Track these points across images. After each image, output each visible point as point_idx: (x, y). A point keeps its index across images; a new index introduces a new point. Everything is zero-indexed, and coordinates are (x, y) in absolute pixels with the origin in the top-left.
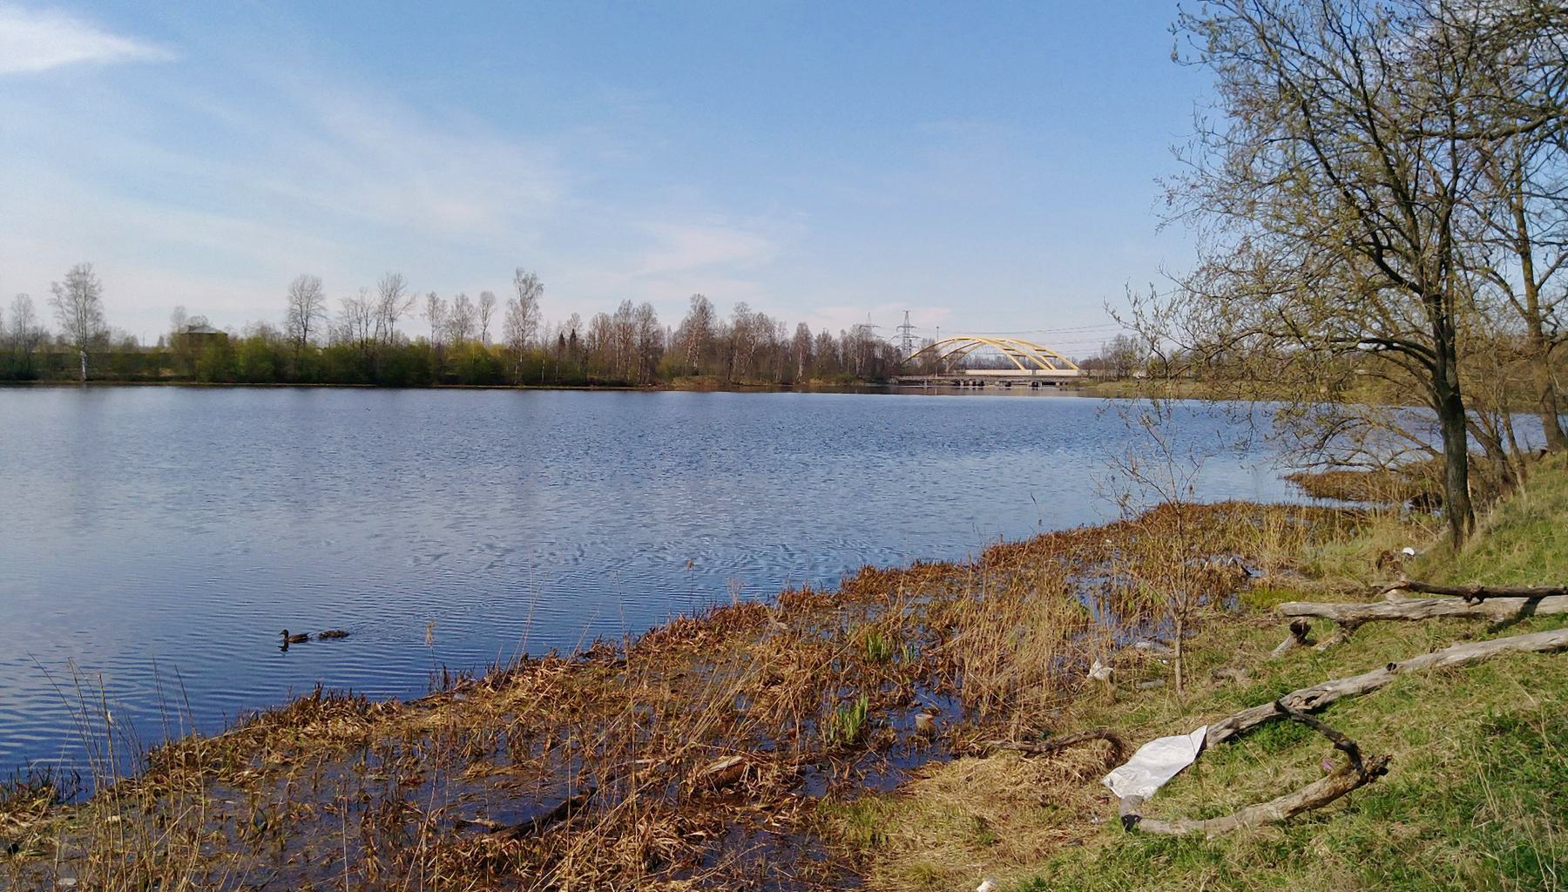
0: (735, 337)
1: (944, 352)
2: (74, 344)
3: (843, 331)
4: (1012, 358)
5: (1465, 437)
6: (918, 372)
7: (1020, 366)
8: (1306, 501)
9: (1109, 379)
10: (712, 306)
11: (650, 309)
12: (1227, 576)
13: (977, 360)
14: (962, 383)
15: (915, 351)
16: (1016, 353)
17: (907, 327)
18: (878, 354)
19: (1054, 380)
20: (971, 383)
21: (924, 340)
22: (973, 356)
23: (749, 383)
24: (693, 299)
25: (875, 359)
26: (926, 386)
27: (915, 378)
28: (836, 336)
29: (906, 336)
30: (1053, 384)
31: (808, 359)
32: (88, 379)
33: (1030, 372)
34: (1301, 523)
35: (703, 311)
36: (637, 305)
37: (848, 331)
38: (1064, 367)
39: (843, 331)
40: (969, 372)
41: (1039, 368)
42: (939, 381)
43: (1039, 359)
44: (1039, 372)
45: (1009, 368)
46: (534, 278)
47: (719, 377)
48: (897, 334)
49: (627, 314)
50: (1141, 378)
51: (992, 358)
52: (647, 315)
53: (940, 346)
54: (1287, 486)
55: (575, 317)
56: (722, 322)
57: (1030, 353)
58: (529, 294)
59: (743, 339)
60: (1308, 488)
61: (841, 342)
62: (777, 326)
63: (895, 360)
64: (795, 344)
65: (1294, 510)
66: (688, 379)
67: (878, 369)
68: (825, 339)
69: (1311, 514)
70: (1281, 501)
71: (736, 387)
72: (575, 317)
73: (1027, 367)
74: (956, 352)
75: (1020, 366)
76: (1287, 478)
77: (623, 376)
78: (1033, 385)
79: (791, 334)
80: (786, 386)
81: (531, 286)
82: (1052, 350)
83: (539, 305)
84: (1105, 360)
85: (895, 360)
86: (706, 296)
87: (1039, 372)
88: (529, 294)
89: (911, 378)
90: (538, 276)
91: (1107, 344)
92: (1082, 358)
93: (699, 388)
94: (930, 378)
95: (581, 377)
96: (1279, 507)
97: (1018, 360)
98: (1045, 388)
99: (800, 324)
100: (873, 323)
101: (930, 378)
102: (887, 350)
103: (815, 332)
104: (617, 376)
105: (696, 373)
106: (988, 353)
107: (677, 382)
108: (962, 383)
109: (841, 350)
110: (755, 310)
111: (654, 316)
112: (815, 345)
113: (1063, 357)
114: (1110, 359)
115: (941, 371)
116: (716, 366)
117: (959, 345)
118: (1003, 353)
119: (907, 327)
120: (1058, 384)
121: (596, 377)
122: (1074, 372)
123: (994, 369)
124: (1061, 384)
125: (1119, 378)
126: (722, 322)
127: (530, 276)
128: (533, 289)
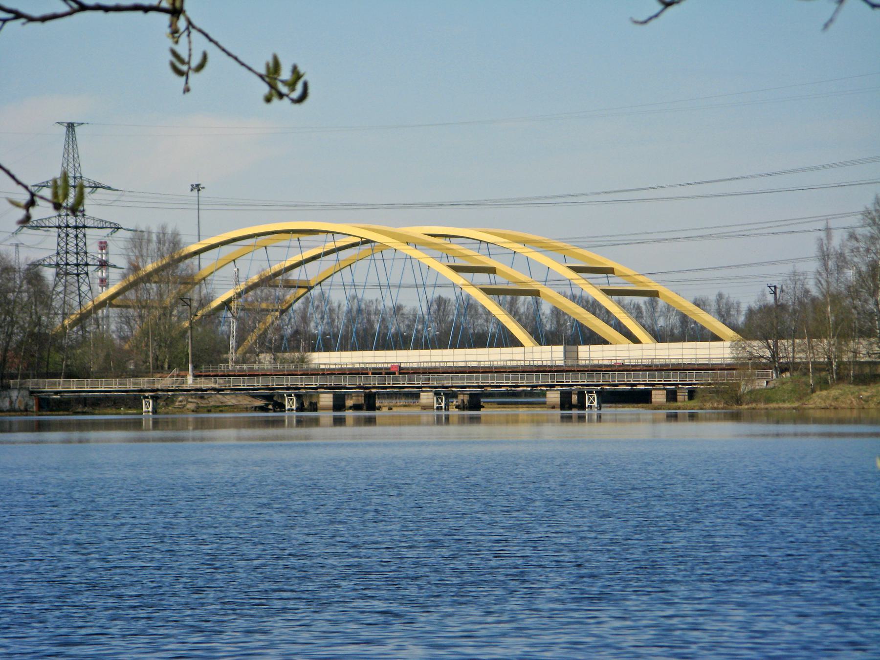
2: (865, 372)
5: (741, 336)
13: (358, 313)
14: (290, 404)
16: (499, 282)
19: (641, 382)
20: (326, 399)
21: (139, 239)
22: (338, 298)
26: (147, 407)
27: (102, 386)
30: (641, 398)
32: (856, 377)
33: (555, 354)
40: (321, 359)
42: (200, 393)
43: (593, 307)
44: (588, 354)
45: (480, 341)
53: (207, 261)
63: (24, 319)
73: (543, 338)
74: (267, 281)
78: (565, 403)
84: (835, 299)
85: (24, 319)
87: (588, 354)
89: (86, 386)
91: (837, 241)
94: (165, 382)
97: (513, 311)
98: (609, 411)
101: (165, 382)
108: (290, 404)
114: (853, 292)
120: (658, 396)
123: (440, 343)
124: (672, 396)
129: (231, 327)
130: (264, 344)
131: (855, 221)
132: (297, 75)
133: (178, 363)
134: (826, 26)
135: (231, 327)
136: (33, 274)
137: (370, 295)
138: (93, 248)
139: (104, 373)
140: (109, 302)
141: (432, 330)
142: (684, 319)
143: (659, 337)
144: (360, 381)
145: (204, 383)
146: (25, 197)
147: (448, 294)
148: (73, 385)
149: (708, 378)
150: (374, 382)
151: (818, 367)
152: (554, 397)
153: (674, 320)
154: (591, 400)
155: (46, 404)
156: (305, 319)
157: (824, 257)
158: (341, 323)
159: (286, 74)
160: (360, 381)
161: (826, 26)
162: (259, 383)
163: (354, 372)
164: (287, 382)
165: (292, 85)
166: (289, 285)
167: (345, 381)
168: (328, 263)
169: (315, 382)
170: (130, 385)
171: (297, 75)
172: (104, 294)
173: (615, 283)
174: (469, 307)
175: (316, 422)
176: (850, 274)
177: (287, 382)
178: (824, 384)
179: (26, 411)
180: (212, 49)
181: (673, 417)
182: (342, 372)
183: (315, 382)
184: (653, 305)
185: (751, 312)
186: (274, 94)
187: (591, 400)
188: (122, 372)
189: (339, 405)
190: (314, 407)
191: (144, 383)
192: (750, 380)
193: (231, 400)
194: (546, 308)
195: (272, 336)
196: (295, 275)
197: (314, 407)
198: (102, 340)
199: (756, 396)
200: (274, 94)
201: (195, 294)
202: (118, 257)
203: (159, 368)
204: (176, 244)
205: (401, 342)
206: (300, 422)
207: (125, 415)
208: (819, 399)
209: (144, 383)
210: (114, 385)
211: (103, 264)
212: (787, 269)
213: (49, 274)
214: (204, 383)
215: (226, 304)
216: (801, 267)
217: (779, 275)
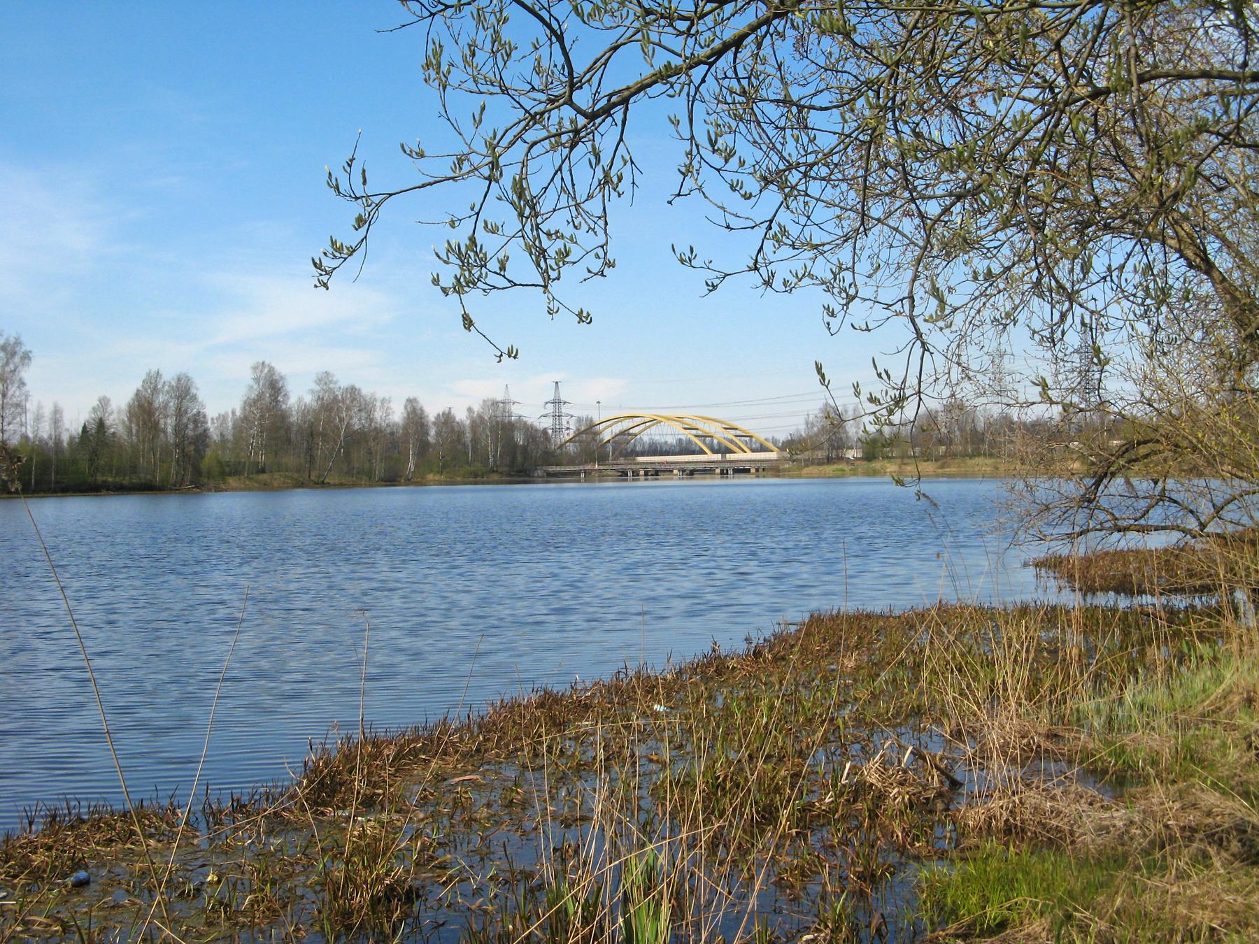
0: (317, 419)
1: (607, 436)
3: (470, 410)
4: (696, 440)
6: (572, 461)
7: (706, 450)
8: (1072, 599)
9: (820, 463)
10: (282, 378)
11: (189, 380)
12: (897, 796)
14: (630, 474)
15: (566, 436)
16: (700, 433)
17: (557, 402)
18: (520, 439)
20: (642, 472)
21: (579, 420)
23: (337, 481)
24: (255, 368)
25: (516, 446)
28: (461, 416)
29: (557, 416)
30: (747, 471)
31: (424, 447)
33: (718, 457)
34: (1074, 642)
35: (273, 386)
36: (169, 376)
37: (477, 408)
38: (763, 449)
39: (470, 410)
40: (640, 459)
41: (731, 452)
43: (731, 441)
45: (693, 453)
46: (18, 342)
47: (296, 475)
48: (545, 412)
49: (155, 390)
50: (857, 459)
51: (671, 440)
52: (183, 391)
54: (1037, 576)
55: (104, 402)
56: (300, 400)
57: (719, 434)
58: (12, 367)
59: (329, 421)
60: (1071, 577)
61: (468, 422)
62: (378, 404)
63: (542, 447)
64: (406, 427)
65: (1052, 616)
66: (251, 479)
67: (519, 459)
68: (446, 420)
69: (1093, 621)
70: (1028, 598)
71: (321, 484)
72: (104, 402)
73: (714, 451)
75: (706, 450)
76: (1038, 565)
77: (149, 477)
78: (722, 473)
79: (397, 415)
80: (392, 479)
81: (14, 354)
82: (745, 426)
83: (26, 380)
84: (811, 437)
85: (542, 447)
86: (273, 365)
87: (729, 457)
88: (12, 367)
89: (559, 468)
90: (23, 339)
92: (782, 437)
93: (266, 487)
94: (588, 467)
95: (90, 480)
96: (1024, 611)
97: (704, 442)
98: (736, 475)
99: (409, 401)
100: (513, 398)
101: (588, 467)
102: (530, 432)
103: (432, 412)
104: (143, 477)
105: (263, 471)
106: (668, 434)
107: (232, 481)
108: (630, 474)
109: (468, 435)
110: (343, 381)
111: (193, 391)
112: (433, 432)
113: (761, 436)
114: (817, 435)
115: (603, 458)
116: (290, 460)
117: (626, 424)
118: (688, 435)
119: (557, 402)
120: (753, 471)
121: (110, 479)
122: (773, 456)
123: (680, 453)
124: (757, 470)
125: (829, 460)
126: (300, 400)
127: (12, 340)
128: (17, 359)
129: (610, 448)
130: (621, 455)
131: (817, 412)
132: (589, 315)
133: (592, 461)
134: (819, 369)
135: (610, 448)
136: (545, 431)
137: (657, 438)
138: (564, 423)
139: (568, 464)
140: (570, 441)
141: (678, 449)
142: (761, 445)
143: (753, 451)
144: (653, 466)
145: (601, 467)
146: (499, 354)
147: (683, 437)
148: (559, 468)
149: (769, 464)
150: (658, 467)
151: (805, 460)
152: (718, 471)
153: (758, 445)
154: (731, 472)
155: (550, 475)
156: (635, 446)
157: (807, 423)
158: (647, 447)
159: (585, 314)
160: (653, 466)
161: (819, 369)
162: (619, 467)
163: (651, 463)
164: (629, 467)
165: (587, 318)
166: (629, 434)
167: (649, 466)
168: (642, 427)
169: (638, 467)
170: (577, 468)
171: (589, 315)
172: (567, 438)
173: (738, 433)
174: (689, 442)
175: (638, 480)
176: (815, 429)
177: (629, 467)
178: (807, 466)
179: (543, 477)
180: (561, 306)
181: (758, 477)
182: (647, 463)
183: (638, 467)
184: (751, 440)
185: (783, 442)
186: (581, 320)
187: (731, 472)
188: (574, 464)
189: (646, 474)
190: (638, 475)
191: (581, 467)
192: (783, 464)
193: (610, 473)
194: (715, 441)
195: (624, 452)
196: (631, 431)
197: (638, 475)
198: (567, 453)
199: (785, 470)
200: (581, 320)
201: (598, 438)
202: (573, 427)
203: (586, 462)
204: (591, 421)
205: (667, 453)
206: (633, 480)
207: (575, 478)
208: (805, 471)
209: (581, 467)
210: (572, 468)
211: (568, 428)
212: (795, 428)
213: (550, 432)
214: (601, 467)
215: (609, 441)
216: (800, 427)
217: (792, 430)
